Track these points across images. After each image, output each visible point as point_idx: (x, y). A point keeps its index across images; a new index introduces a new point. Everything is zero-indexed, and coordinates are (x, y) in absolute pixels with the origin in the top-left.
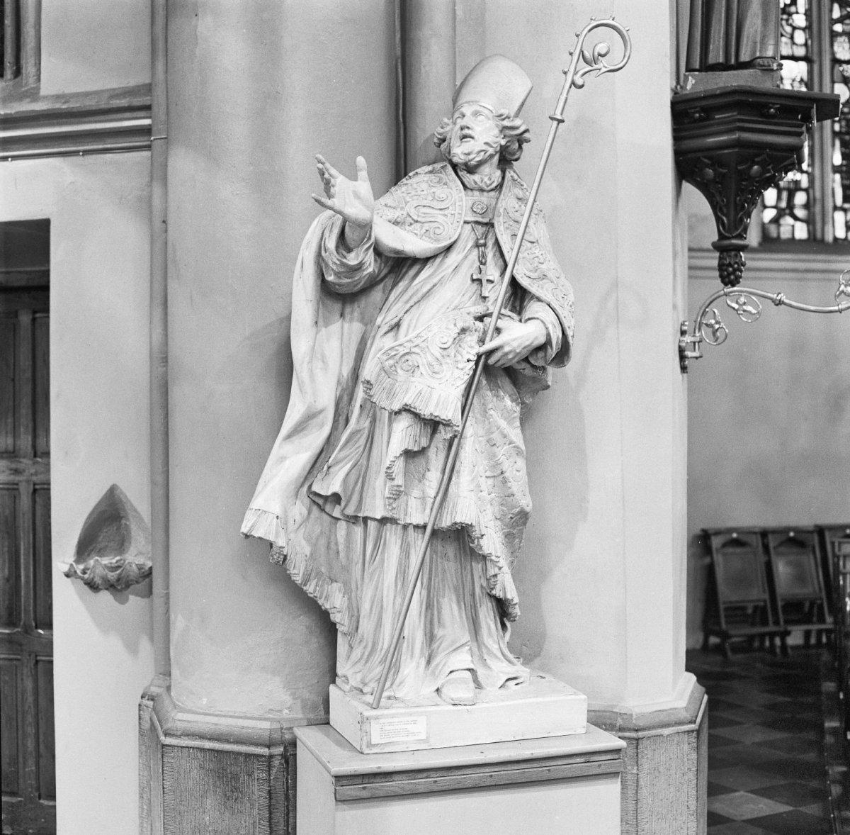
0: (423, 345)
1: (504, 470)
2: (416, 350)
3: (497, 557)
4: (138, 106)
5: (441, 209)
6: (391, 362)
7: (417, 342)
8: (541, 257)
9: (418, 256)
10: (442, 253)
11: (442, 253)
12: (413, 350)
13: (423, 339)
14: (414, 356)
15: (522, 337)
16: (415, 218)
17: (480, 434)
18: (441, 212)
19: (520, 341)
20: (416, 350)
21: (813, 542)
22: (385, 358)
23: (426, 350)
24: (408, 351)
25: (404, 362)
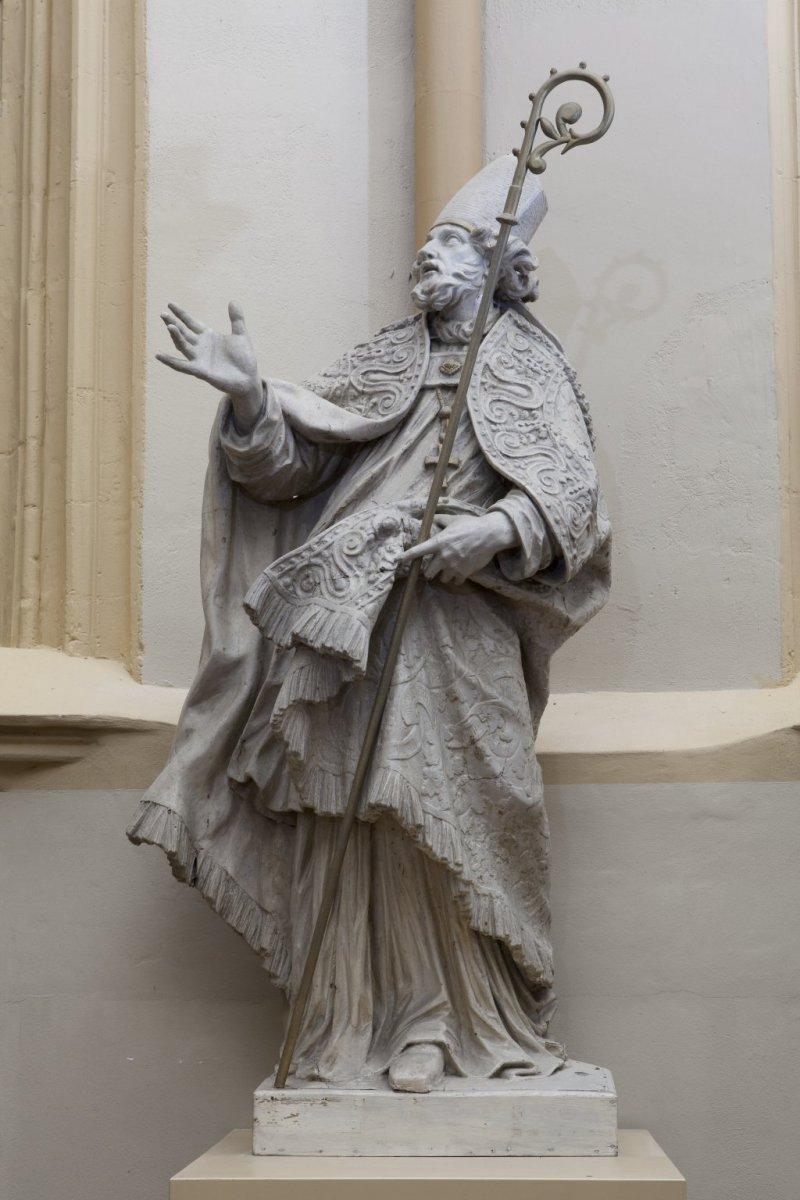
0: (326, 553)
1: (476, 737)
2: (318, 561)
3: (457, 864)
4: (416, 398)
5: (499, 401)
6: (288, 580)
7: (318, 549)
8: (543, 428)
9: (370, 439)
10: (394, 430)
11: (394, 430)
12: (313, 560)
13: (327, 544)
14: (316, 569)
15: (467, 536)
16: (360, 388)
17: (434, 684)
18: (397, 377)
19: (465, 541)
20: (318, 561)
21: (3, 646)
22: (276, 574)
23: (331, 559)
24: (306, 563)
25: (304, 579)
